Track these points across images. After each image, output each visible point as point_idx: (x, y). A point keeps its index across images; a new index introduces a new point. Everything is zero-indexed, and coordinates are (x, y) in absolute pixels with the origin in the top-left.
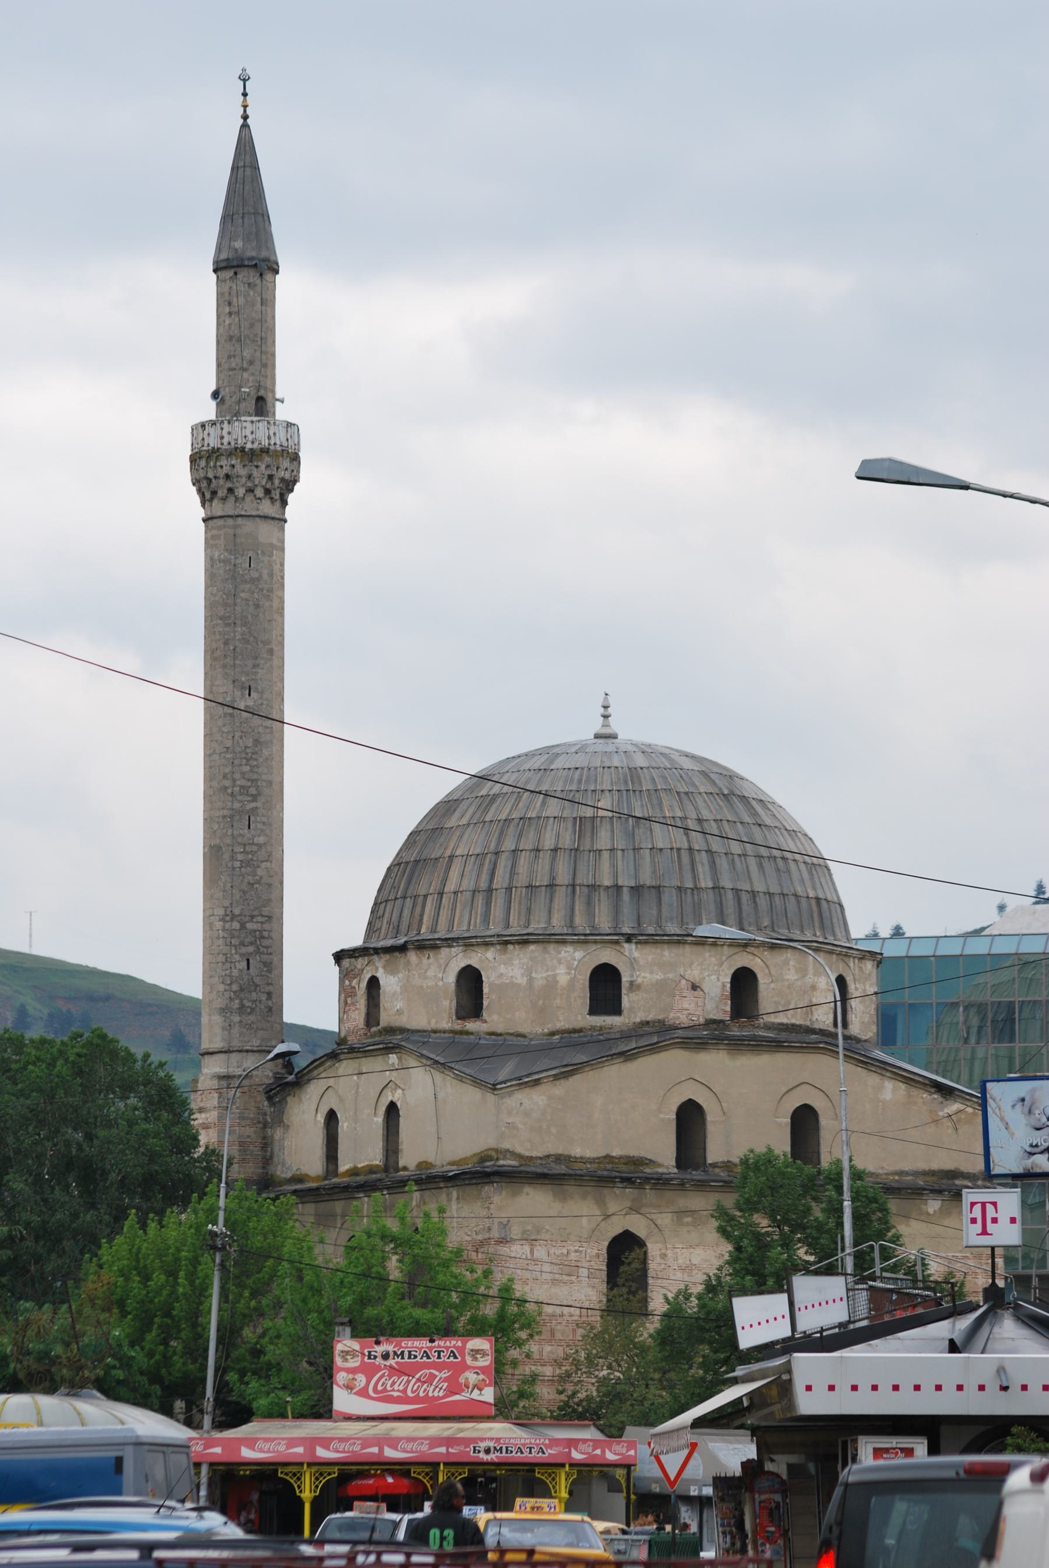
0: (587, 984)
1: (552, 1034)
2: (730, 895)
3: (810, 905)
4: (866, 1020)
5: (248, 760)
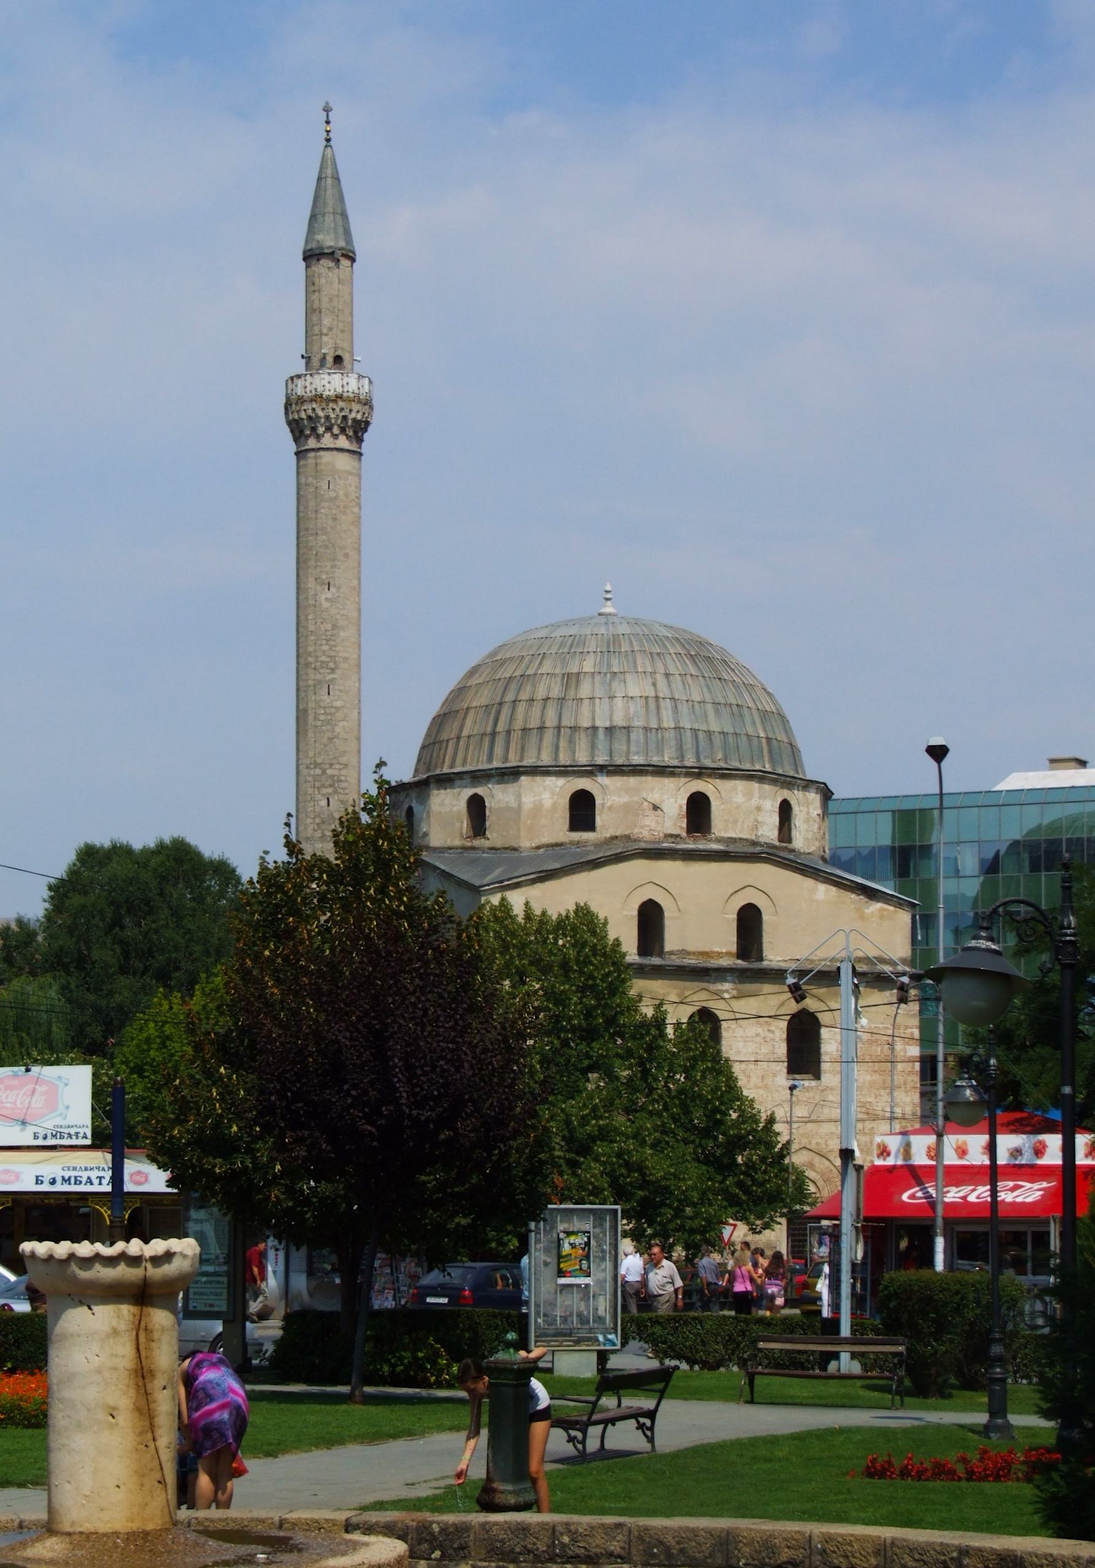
0: (567, 806)
1: (538, 848)
2: (689, 734)
3: (760, 742)
4: (810, 836)
5: (328, 641)
